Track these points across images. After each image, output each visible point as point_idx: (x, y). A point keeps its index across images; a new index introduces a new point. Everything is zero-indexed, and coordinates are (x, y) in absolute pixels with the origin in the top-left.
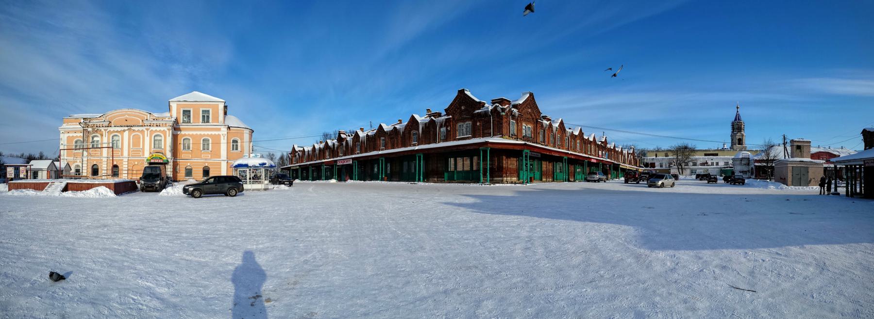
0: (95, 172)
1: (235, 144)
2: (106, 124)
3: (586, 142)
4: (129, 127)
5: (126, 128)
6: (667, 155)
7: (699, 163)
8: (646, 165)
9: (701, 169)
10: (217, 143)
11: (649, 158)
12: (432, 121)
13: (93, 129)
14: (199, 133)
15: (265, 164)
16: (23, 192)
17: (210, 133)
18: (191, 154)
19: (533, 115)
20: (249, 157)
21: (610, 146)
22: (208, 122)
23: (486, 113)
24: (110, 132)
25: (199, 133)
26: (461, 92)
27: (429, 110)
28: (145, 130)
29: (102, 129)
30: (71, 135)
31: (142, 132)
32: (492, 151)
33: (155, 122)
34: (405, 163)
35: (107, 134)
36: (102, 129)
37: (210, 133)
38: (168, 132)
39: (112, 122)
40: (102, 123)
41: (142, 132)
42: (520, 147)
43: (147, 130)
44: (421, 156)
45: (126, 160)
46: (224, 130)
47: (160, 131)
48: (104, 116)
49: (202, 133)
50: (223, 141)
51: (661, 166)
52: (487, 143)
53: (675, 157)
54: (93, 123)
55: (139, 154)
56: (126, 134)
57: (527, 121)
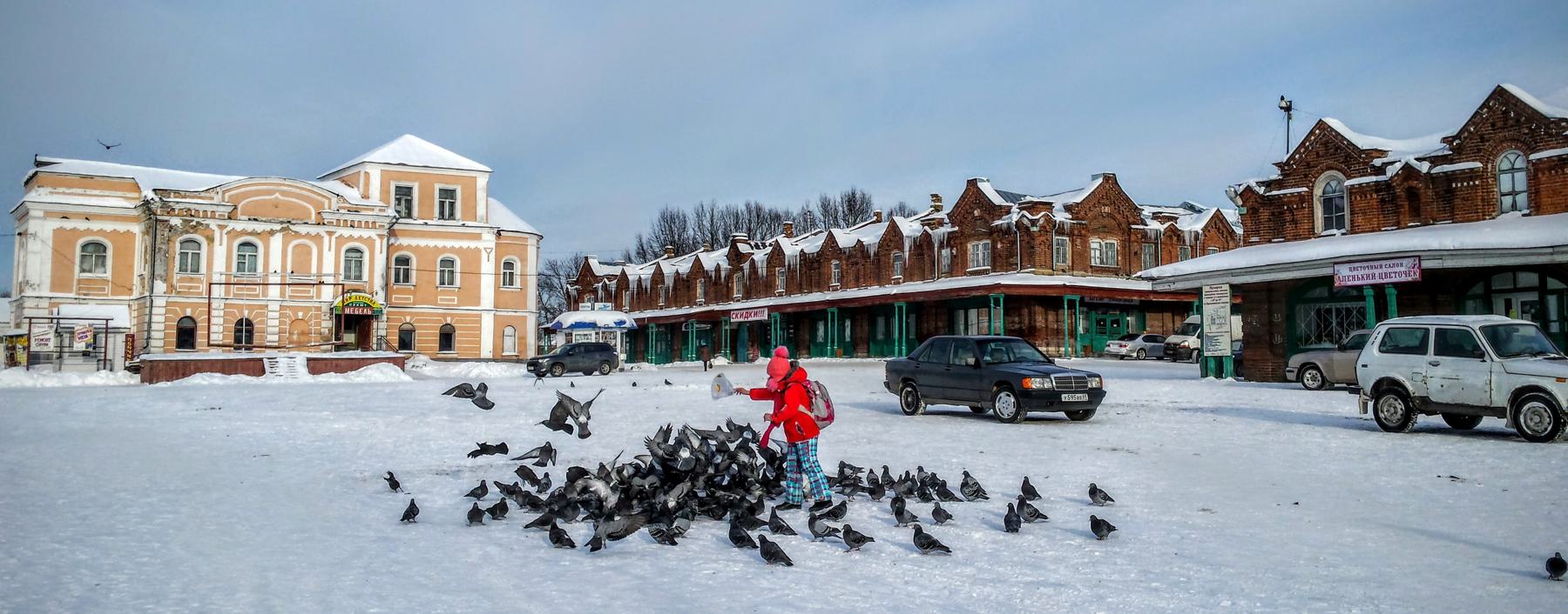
0: (186, 335)
1: (508, 271)
2: (225, 210)
4: (285, 225)
5: (278, 227)
10: (473, 273)
12: (926, 235)
13: (184, 221)
14: (432, 243)
15: (624, 323)
16: (204, 379)
17: (457, 244)
18: (414, 293)
19: (1118, 217)
20: (593, 309)
22: (452, 216)
24: (233, 234)
25: (432, 243)
26: (972, 183)
27: (936, 196)
28: (323, 234)
29: (213, 224)
30: (68, 225)
31: (317, 238)
32: (1008, 298)
33: (349, 217)
34: (881, 322)
35: (225, 237)
37: (457, 244)
38: (378, 242)
39: (239, 207)
40: (215, 208)
41: (317, 238)
42: (1056, 291)
43: (330, 234)
44: (902, 307)
45: (274, 306)
46: (489, 240)
47: (360, 239)
48: (218, 189)
49: (440, 243)
50: (488, 267)
52: (998, 286)
54: (188, 206)
55: (198, 288)
56: (276, 242)
57: (1104, 231)
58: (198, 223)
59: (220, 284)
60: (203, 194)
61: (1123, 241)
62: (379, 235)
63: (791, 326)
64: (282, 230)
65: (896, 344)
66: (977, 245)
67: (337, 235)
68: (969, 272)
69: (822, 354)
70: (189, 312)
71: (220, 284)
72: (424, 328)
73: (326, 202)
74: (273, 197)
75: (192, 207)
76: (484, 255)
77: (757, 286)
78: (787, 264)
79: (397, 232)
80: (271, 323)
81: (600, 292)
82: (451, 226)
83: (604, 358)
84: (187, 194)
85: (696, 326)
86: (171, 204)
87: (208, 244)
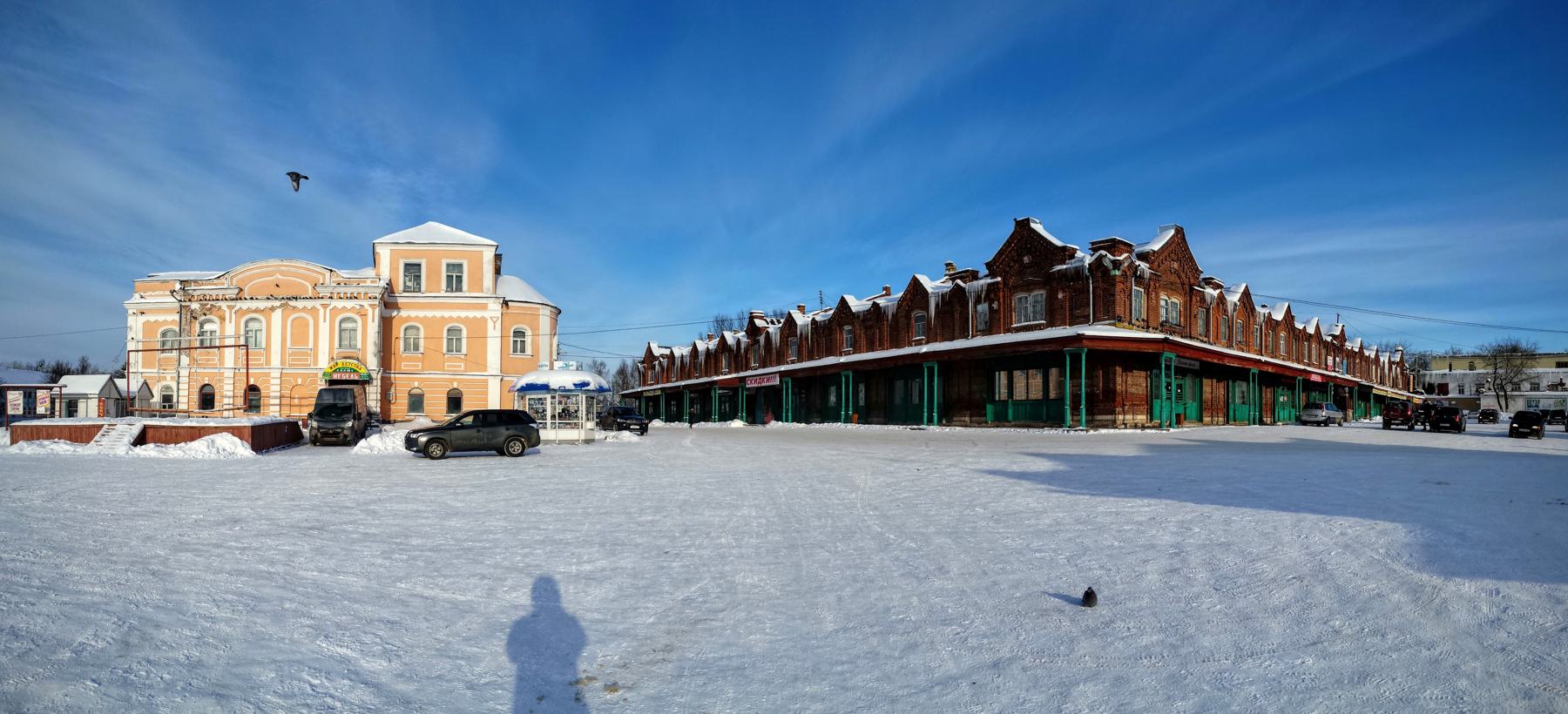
0: (207, 400)
3: (1300, 336)
4: (283, 302)
5: (277, 303)
6: (1472, 368)
7: (1544, 383)
8: (1430, 389)
9: (1550, 397)
10: (479, 336)
11: (1435, 374)
12: (958, 290)
14: (438, 314)
15: (588, 384)
19: (1183, 276)
20: (552, 368)
21: (1353, 345)
22: (459, 289)
23: (1078, 273)
24: (240, 313)
25: (438, 314)
32: (1092, 354)
35: (233, 316)
36: (223, 305)
41: (314, 310)
43: (325, 306)
45: (276, 374)
49: (447, 314)
51: (1461, 391)
53: (1490, 370)
56: (277, 316)
57: (1171, 288)
58: (212, 305)
59: (137, 351)
60: (215, 281)
61: (1185, 303)
62: (370, 305)
63: (804, 391)
64: (281, 306)
65: (843, 409)
66: (1026, 298)
67: (331, 307)
68: (1015, 328)
69: (837, 419)
70: (455, 386)
71: (137, 351)
72: (431, 392)
73: (321, 278)
74: (274, 277)
75: (206, 292)
76: (490, 324)
77: (772, 354)
78: (798, 333)
79: (399, 305)
80: (273, 388)
81: (657, 366)
82: (454, 298)
83: (511, 432)
84: (204, 282)
85: (718, 392)
86: (190, 292)
87: (221, 323)
